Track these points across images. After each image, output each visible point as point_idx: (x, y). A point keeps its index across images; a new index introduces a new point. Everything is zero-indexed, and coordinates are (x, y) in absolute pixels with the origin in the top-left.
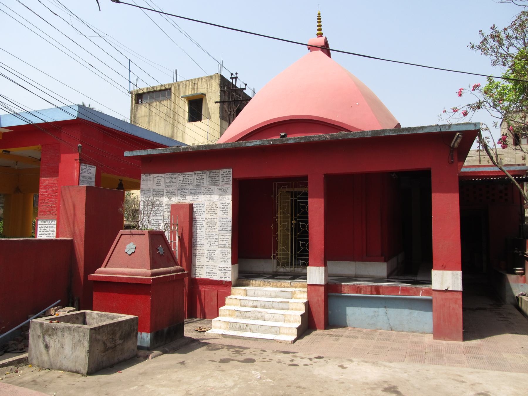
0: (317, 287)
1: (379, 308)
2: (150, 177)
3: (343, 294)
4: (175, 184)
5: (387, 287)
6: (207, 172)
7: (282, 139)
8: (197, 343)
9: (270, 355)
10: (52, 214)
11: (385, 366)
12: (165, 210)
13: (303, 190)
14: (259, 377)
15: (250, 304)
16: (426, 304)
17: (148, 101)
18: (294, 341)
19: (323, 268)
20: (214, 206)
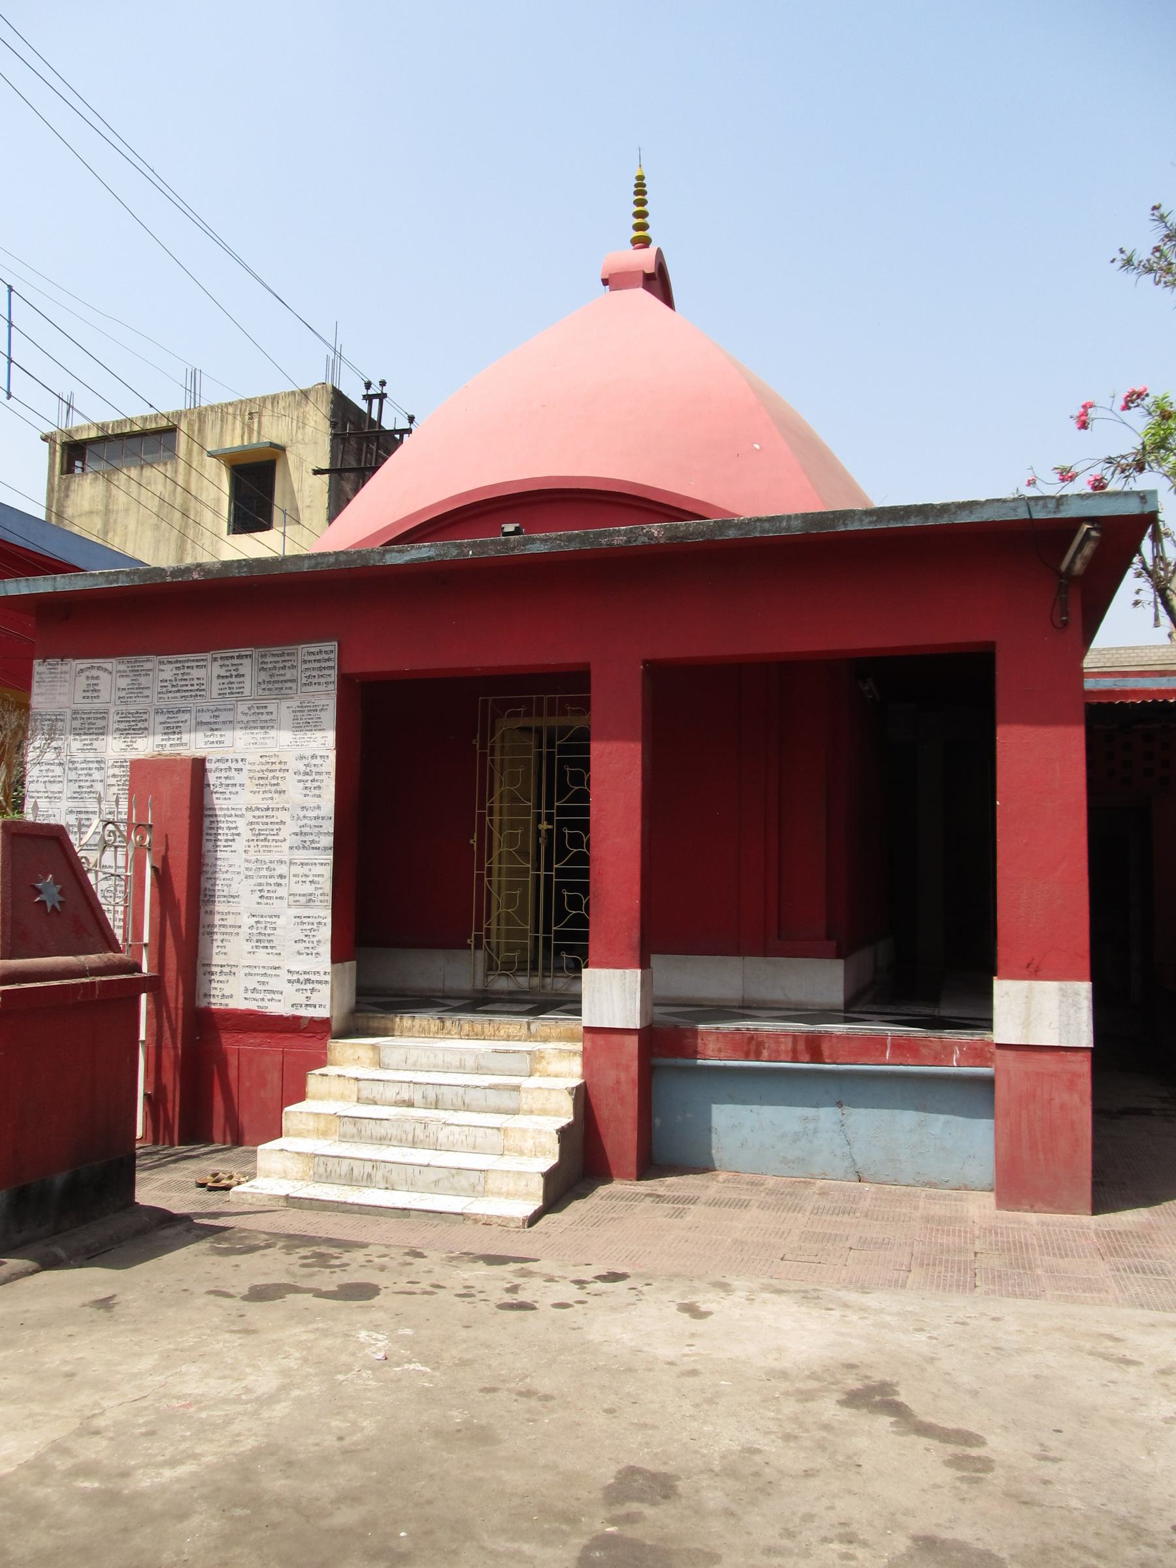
0: (616, 1038)
1: (817, 1106)
2: (65, 668)
3: (700, 1062)
4: (146, 693)
5: (847, 1038)
6: (255, 652)
7: (507, 541)
8: (180, 1228)
9: (437, 1269)
11: (846, 1305)
12: (113, 781)
13: (577, 723)
14: (380, 1355)
15: (390, 1093)
16: (976, 1094)
17: (102, 466)
18: (533, 1220)
19: (634, 975)
20: (277, 767)
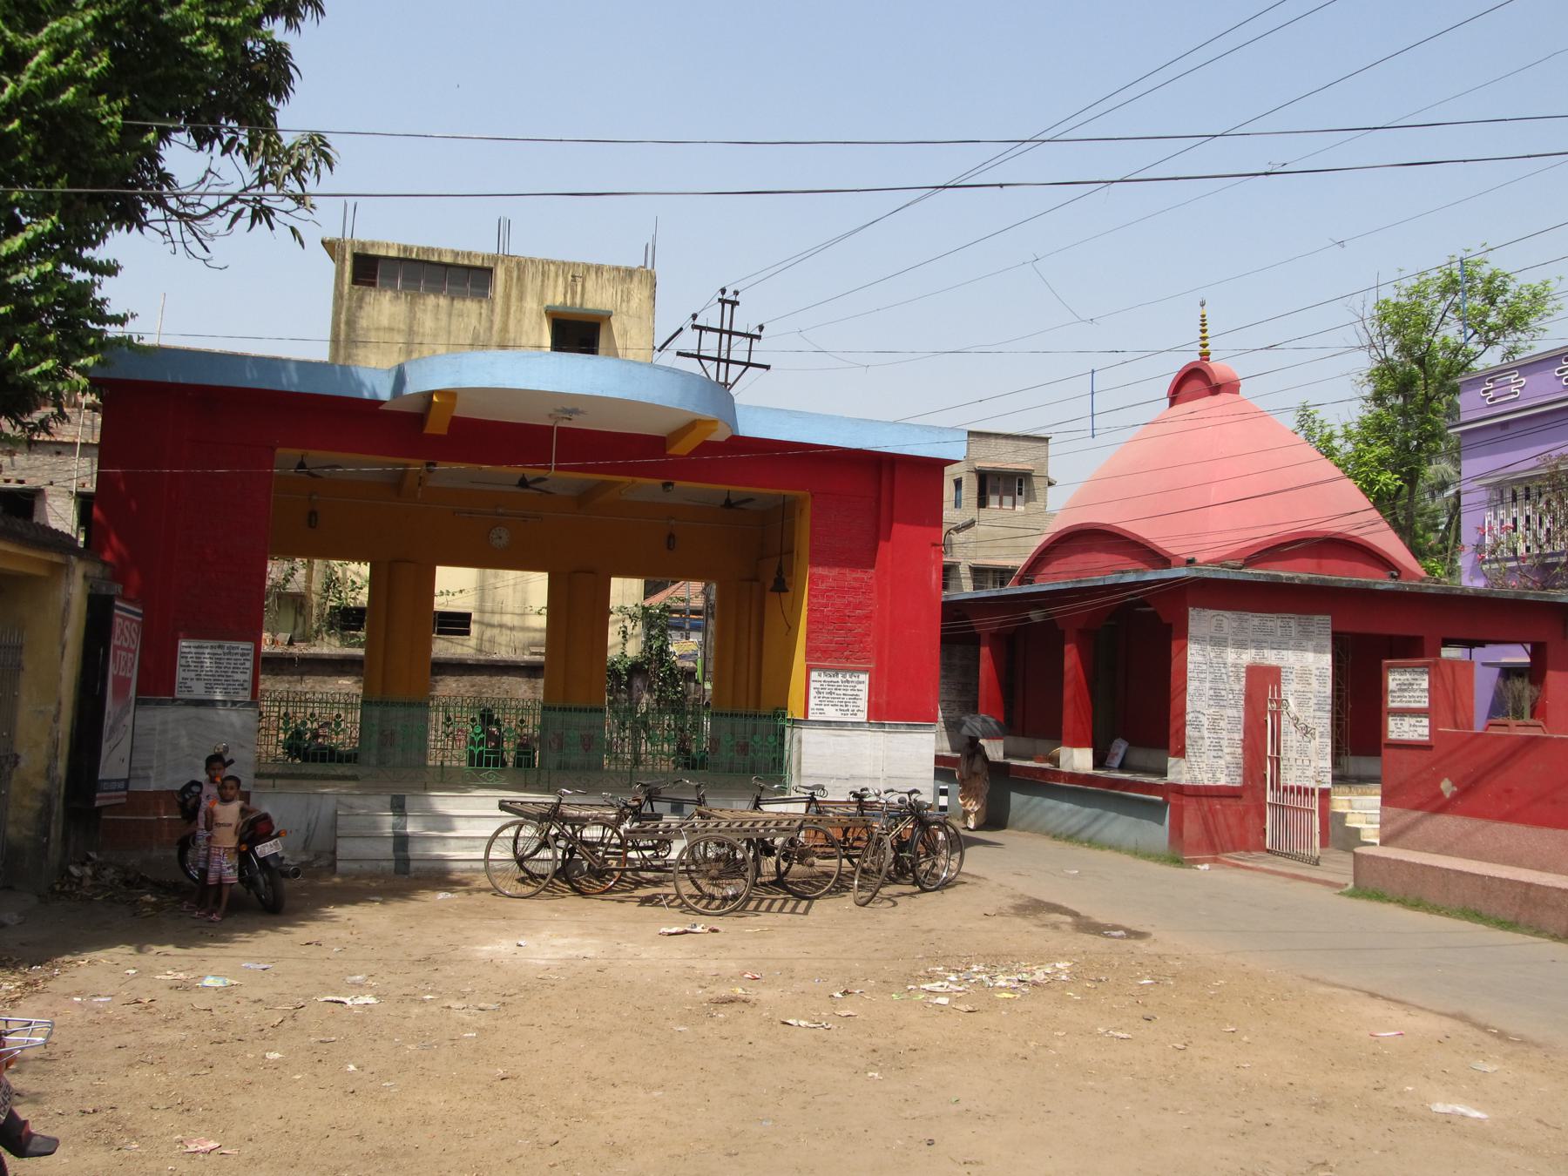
10: (847, 658)
